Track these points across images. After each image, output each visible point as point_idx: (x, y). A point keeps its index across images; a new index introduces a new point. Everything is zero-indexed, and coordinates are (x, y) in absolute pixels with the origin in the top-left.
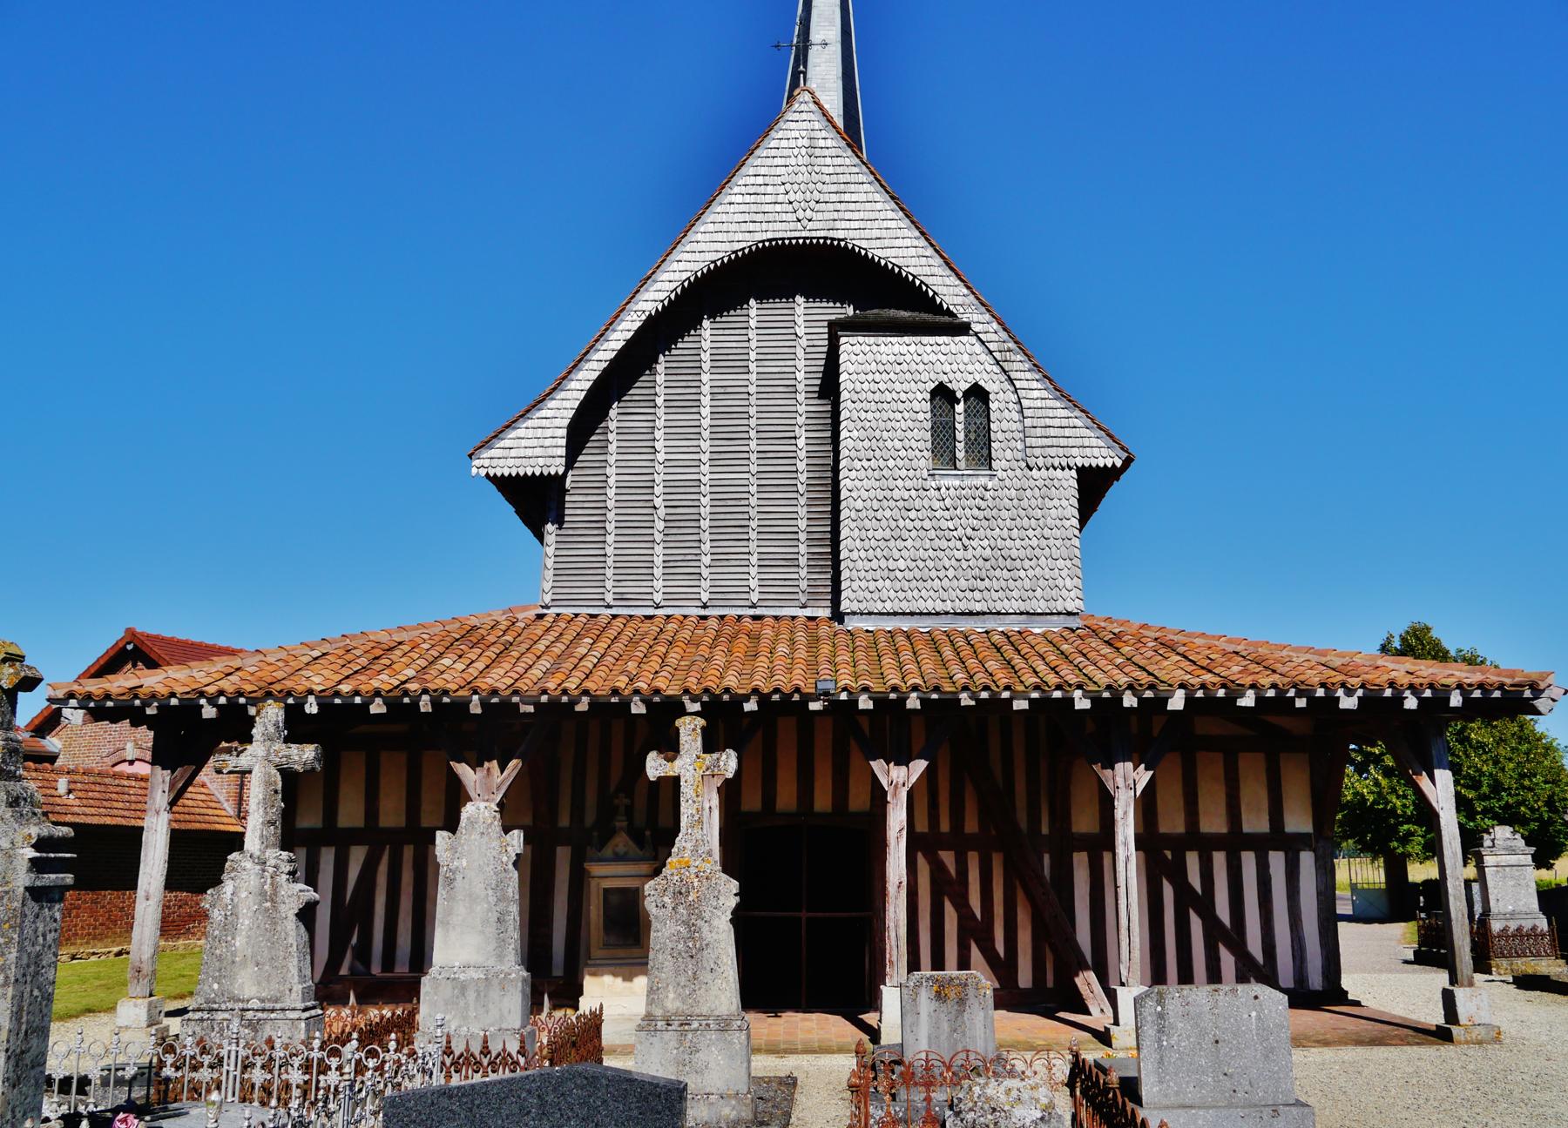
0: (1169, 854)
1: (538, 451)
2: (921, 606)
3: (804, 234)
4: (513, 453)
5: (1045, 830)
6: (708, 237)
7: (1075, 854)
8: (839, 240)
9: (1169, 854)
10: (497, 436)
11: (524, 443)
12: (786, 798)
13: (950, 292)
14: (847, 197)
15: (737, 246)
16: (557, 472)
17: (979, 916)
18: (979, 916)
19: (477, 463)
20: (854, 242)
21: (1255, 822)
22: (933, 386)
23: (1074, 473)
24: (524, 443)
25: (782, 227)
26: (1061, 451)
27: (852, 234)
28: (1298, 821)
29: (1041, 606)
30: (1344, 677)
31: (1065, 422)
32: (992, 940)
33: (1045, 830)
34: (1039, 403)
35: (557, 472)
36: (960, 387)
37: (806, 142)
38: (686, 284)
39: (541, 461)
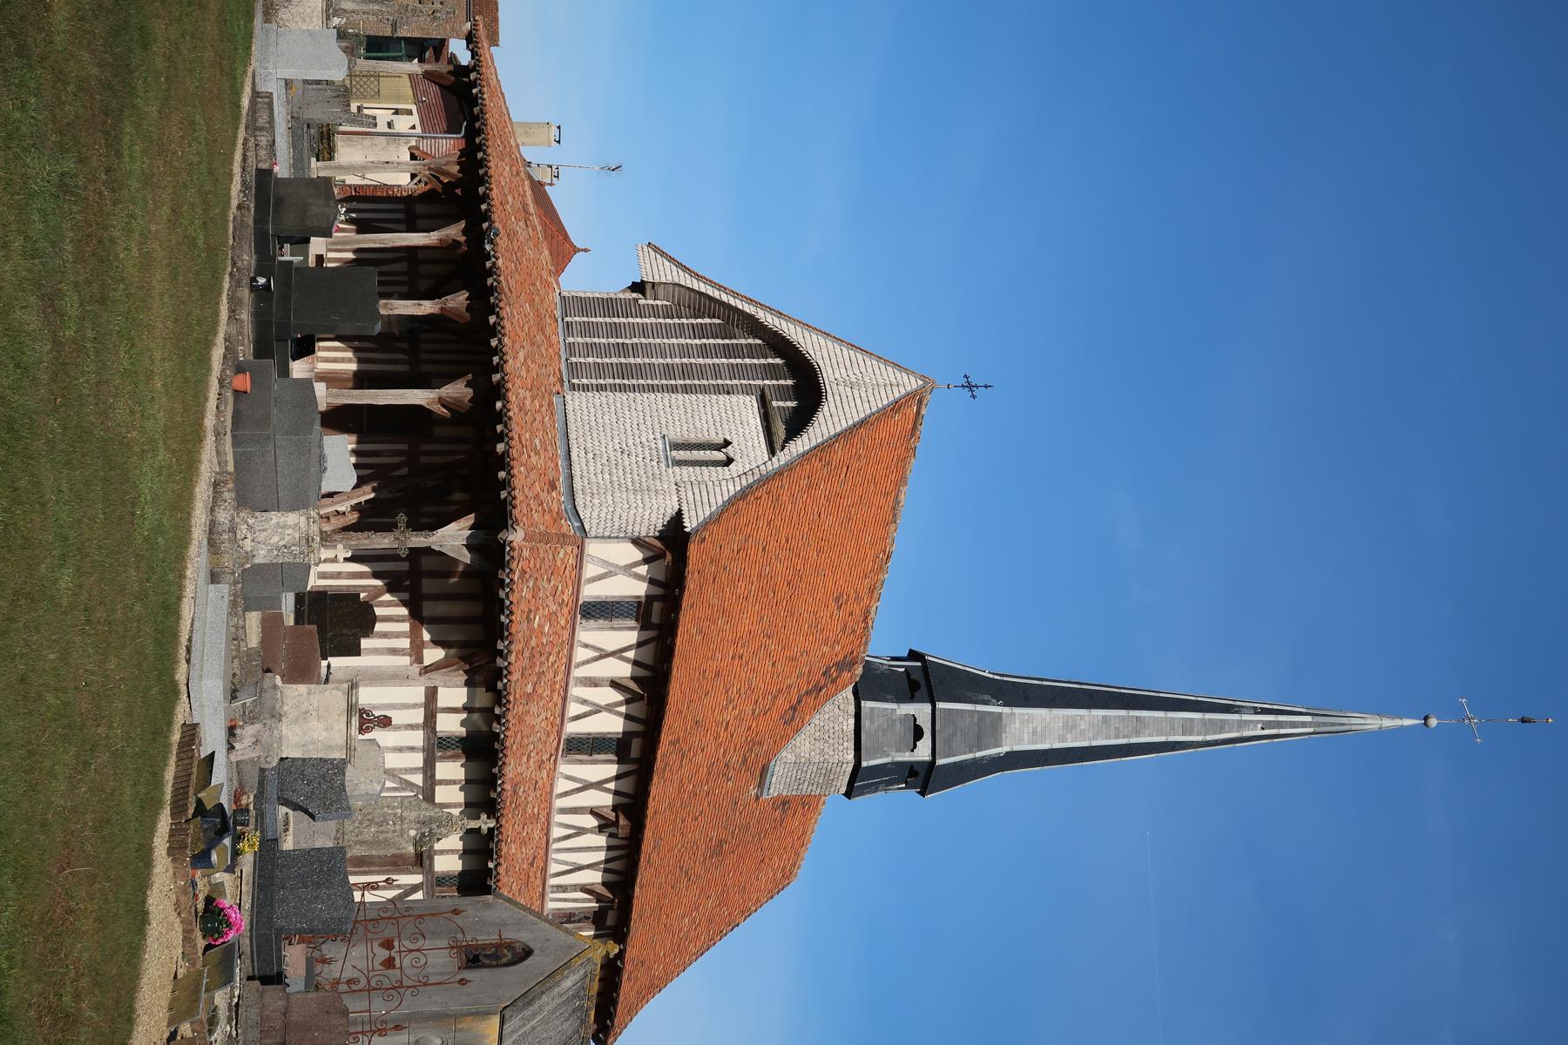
0: (408, 583)
2: (572, 427)
3: (826, 382)
7: (408, 594)
8: (826, 398)
9: (408, 583)
10: (663, 254)
11: (661, 268)
13: (801, 445)
14: (858, 401)
15: (812, 352)
24: (661, 268)
25: (829, 375)
30: (511, 203)
34: (724, 488)
37: (894, 382)
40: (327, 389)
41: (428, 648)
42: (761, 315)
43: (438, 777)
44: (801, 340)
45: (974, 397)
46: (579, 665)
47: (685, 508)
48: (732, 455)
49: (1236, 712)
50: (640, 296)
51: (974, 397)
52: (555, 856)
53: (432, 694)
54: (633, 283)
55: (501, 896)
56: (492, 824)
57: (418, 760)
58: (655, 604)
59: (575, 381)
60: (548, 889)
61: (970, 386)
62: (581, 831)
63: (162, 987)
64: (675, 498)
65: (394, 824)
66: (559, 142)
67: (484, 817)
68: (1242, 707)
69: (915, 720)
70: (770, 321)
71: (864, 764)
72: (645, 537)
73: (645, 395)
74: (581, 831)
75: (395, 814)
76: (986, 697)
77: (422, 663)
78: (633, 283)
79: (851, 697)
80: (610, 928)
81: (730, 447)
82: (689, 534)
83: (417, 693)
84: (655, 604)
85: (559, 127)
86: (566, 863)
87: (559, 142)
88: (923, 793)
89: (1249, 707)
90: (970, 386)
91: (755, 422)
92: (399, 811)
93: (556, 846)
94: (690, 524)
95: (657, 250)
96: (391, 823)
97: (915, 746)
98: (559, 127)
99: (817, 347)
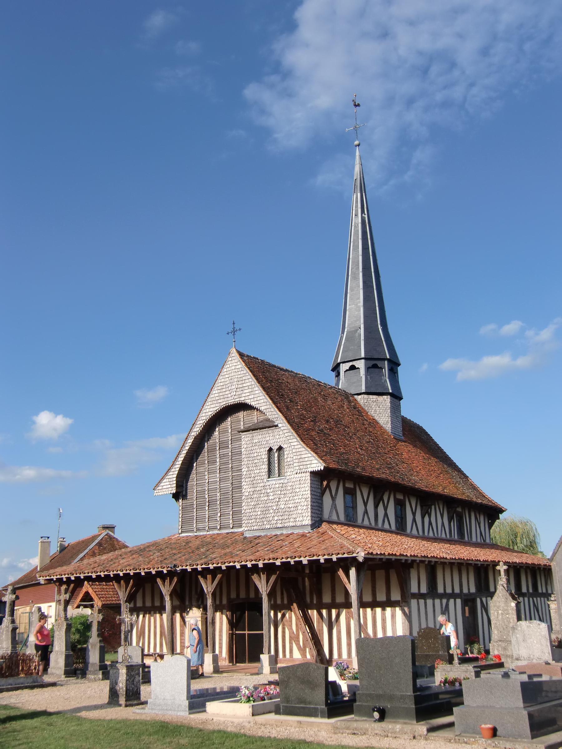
1: (169, 486)
4: (164, 487)
5: (315, 602)
6: (209, 407)
12: (243, 595)
16: (321, 469)
17: (295, 633)
18: (295, 633)
19: (156, 491)
20: (247, 401)
21: (148, 604)
22: (268, 448)
23: (309, 474)
26: (305, 467)
27: (247, 398)
28: (396, 596)
29: (298, 524)
31: (306, 456)
32: (299, 641)
33: (315, 602)
35: (318, 470)
36: (275, 448)
38: (204, 424)
39: (170, 489)
40: (263, 654)
41: (391, 598)
42: (194, 434)
43: (451, 592)
44: (210, 413)
45: (240, 329)
46: (370, 524)
47: (310, 470)
48: (278, 447)
49: (358, 225)
50: (181, 494)
51: (240, 329)
52: (439, 536)
53: (414, 596)
54: (173, 498)
55: (551, 559)
56: (501, 563)
57: (437, 601)
58: (346, 486)
59: (231, 526)
60: (451, 539)
61: (234, 332)
62: (430, 523)
63: (40, 708)
64: (303, 475)
65: (508, 614)
66: (48, 538)
67: (498, 568)
68: (355, 222)
69: (347, 370)
70: (198, 429)
71: (391, 391)
72: (321, 490)
73: (243, 491)
74: (430, 523)
75: (502, 614)
76: (357, 335)
77: (399, 601)
78: (173, 498)
79: (360, 397)
80: (462, 509)
81: (273, 448)
82: (325, 467)
83: (414, 602)
84: (346, 486)
85: (42, 537)
86: (442, 530)
87: (48, 538)
88: (399, 365)
89: (355, 220)
90: (234, 332)
91: (258, 436)
92: (500, 612)
93: (436, 535)
94: (318, 465)
95: (157, 485)
96: (507, 616)
97: (358, 368)
98: (42, 537)
99: (212, 406)
